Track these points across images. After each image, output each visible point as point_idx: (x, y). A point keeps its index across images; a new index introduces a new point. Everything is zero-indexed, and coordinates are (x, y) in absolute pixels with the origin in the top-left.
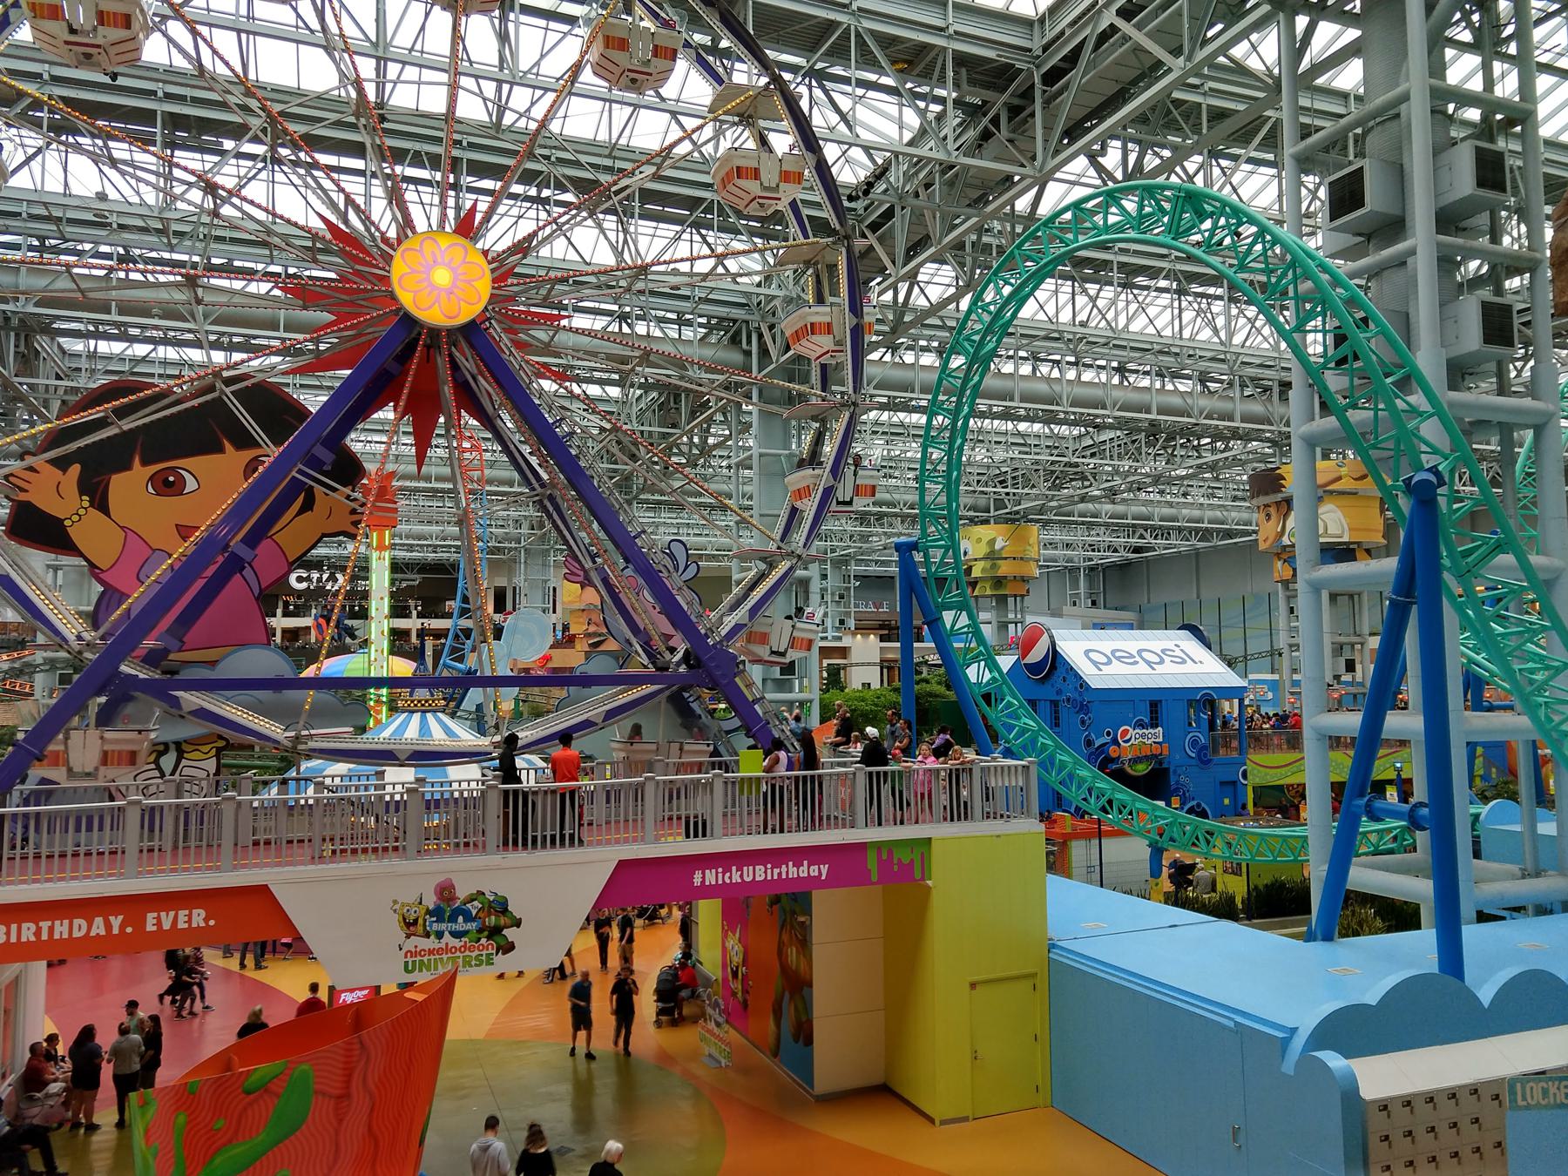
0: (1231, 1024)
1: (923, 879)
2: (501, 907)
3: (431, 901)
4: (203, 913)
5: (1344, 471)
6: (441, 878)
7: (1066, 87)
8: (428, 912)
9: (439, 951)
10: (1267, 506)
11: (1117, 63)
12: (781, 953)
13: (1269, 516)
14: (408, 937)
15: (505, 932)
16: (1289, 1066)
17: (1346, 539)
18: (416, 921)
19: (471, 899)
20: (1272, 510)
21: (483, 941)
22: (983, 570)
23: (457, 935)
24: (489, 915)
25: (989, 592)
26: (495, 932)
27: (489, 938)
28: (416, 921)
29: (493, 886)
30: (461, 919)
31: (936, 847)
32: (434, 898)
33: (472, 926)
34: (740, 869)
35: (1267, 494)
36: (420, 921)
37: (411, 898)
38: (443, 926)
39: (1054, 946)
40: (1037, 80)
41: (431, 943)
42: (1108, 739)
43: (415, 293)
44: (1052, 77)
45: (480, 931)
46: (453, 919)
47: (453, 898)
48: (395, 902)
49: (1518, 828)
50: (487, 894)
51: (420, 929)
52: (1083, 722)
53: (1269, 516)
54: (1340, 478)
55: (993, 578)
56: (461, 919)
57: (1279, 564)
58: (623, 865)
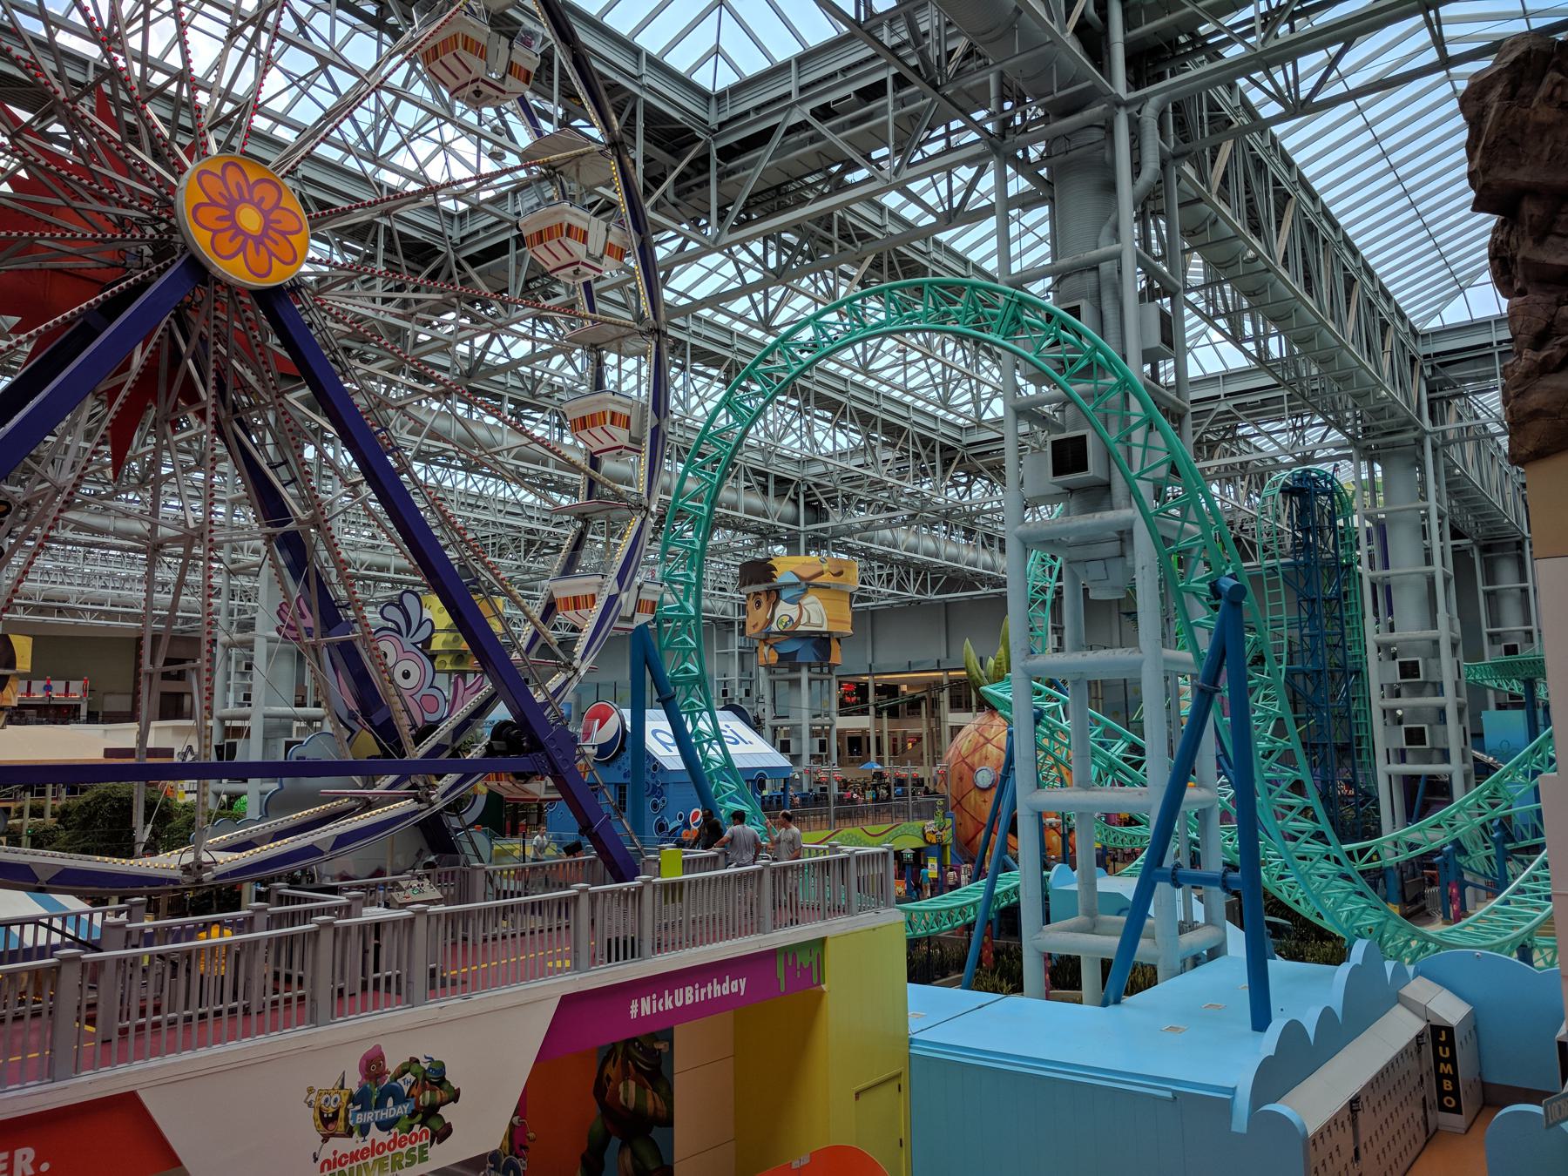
0: (1169, 1095)
1: (819, 984)
2: (435, 1077)
3: (354, 1083)
4: (30, 1153)
5: (825, 567)
6: (367, 1047)
7: (752, 164)
8: (353, 1099)
9: (363, 1154)
10: (757, 594)
11: (798, 160)
12: (600, 1089)
13: (759, 604)
14: (325, 1140)
15: (442, 1111)
16: (1240, 1123)
17: (824, 629)
18: (336, 1114)
19: (403, 1072)
20: (763, 598)
21: (416, 1129)
22: (445, 643)
23: (384, 1126)
24: (424, 1088)
25: (449, 667)
26: (429, 1113)
27: (422, 1123)
28: (336, 1114)
29: (425, 1049)
30: (390, 1101)
31: (829, 945)
32: (359, 1077)
33: (403, 1110)
34: (672, 993)
35: (758, 582)
36: (342, 1114)
37: (330, 1083)
38: (369, 1116)
39: (911, 1041)
40: (714, 153)
41: (353, 1144)
42: (678, 823)
43: (215, 232)
44: (727, 154)
45: (412, 1115)
46: (381, 1104)
47: (382, 1073)
48: (310, 1090)
49: (1075, 887)
50: (422, 1060)
51: (341, 1123)
52: (655, 806)
53: (759, 604)
54: (822, 573)
55: (451, 652)
56: (390, 1101)
57: (766, 649)
58: (566, 1001)
